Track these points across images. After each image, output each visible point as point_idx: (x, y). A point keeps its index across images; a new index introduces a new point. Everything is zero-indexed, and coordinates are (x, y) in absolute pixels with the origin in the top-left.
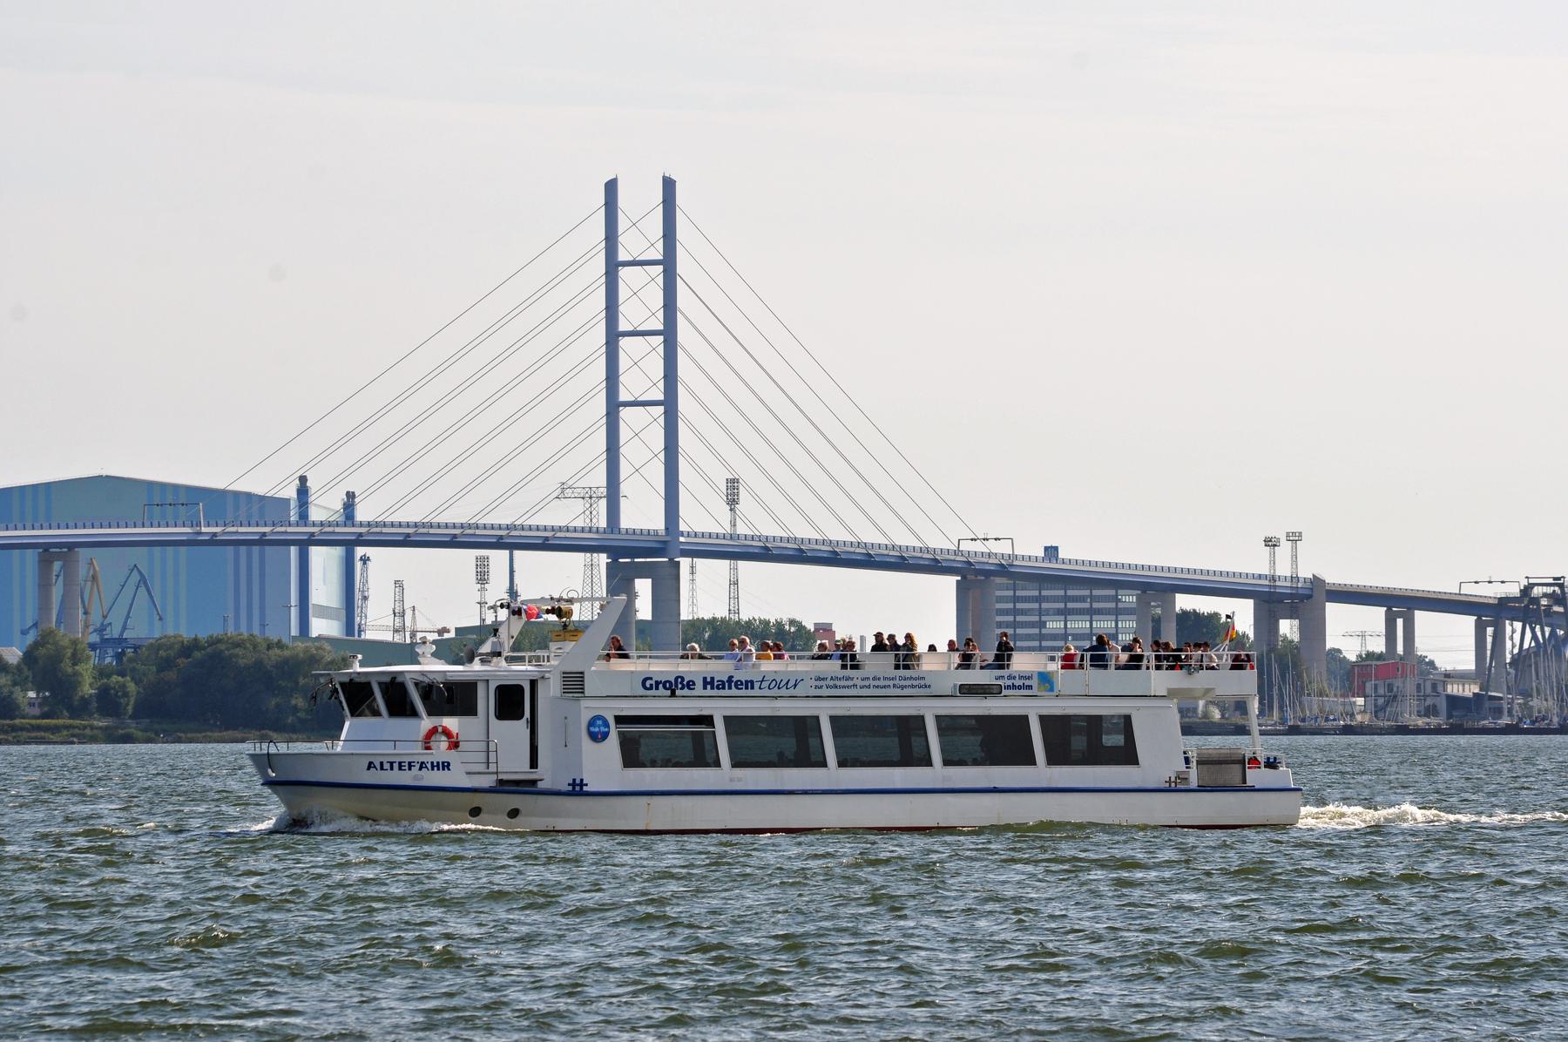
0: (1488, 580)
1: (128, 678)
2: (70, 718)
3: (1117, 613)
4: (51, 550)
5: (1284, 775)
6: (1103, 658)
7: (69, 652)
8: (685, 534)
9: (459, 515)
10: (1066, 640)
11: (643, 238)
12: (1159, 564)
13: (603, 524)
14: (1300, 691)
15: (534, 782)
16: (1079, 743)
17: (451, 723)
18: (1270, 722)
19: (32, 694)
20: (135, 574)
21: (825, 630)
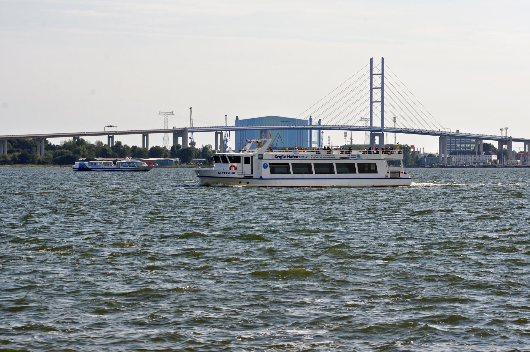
3: (471, 143)
5: (408, 175)
6: (371, 152)
9: (341, 124)
11: (377, 69)
13: (369, 125)
14: (507, 159)
15: (252, 177)
16: (366, 169)
17: (235, 164)
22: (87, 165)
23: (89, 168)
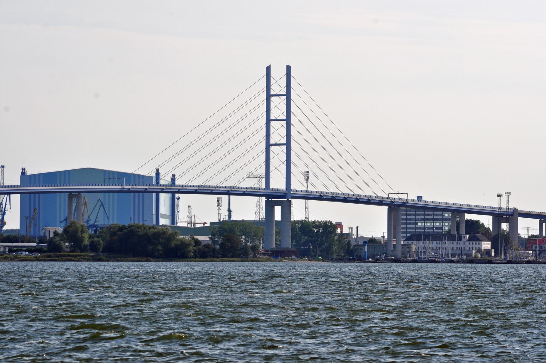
1: (100, 239)
2: (80, 252)
3: (443, 220)
4: (72, 194)
7: (80, 229)
8: (293, 191)
9: (214, 183)
10: (425, 229)
11: (279, 86)
12: (431, 200)
18: (501, 259)
19: (67, 244)
20: (99, 202)
21: (339, 225)
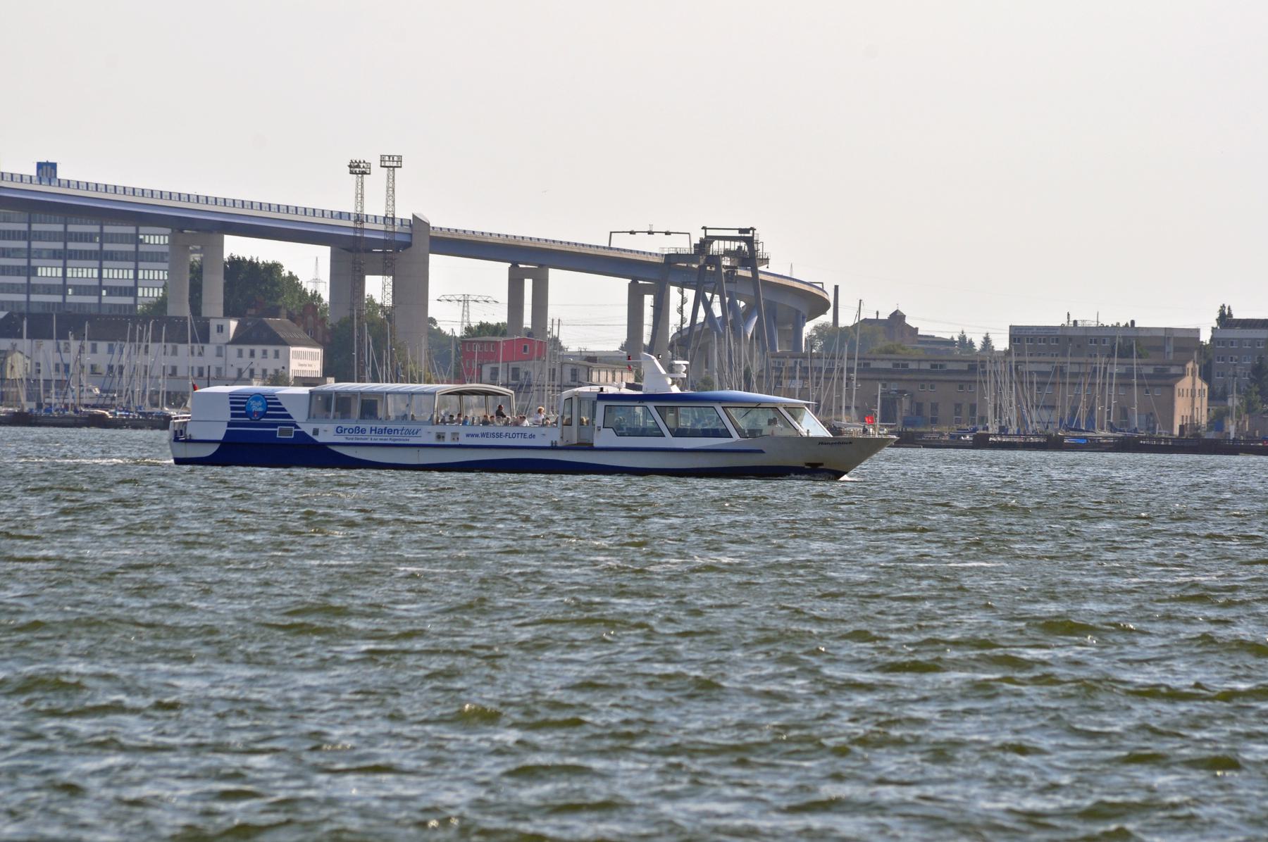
0: (648, 230)
3: (138, 258)
10: (65, 294)
22: (299, 415)
23: (320, 439)
